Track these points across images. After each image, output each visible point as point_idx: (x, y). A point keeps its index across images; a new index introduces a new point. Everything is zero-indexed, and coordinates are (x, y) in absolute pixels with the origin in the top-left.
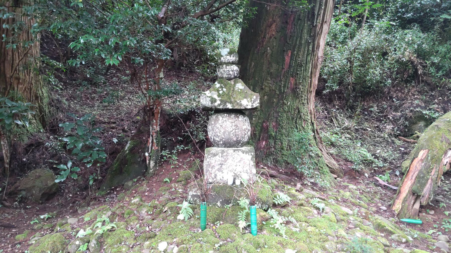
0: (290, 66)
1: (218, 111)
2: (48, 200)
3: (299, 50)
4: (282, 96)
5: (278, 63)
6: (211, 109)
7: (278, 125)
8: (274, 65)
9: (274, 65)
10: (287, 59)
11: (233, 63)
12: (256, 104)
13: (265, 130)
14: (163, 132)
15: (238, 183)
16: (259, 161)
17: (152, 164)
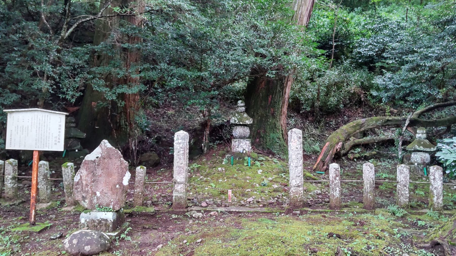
0: (271, 103)
1: (237, 125)
2: (156, 166)
3: (275, 95)
4: (267, 117)
5: (265, 101)
6: (234, 124)
7: (265, 131)
8: (264, 102)
9: (264, 102)
10: (270, 99)
11: (243, 106)
12: (251, 122)
13: (258, 134)
14: (211, 135)
15: (244, 152)
16: (252, 144)
17: (206, 149)
